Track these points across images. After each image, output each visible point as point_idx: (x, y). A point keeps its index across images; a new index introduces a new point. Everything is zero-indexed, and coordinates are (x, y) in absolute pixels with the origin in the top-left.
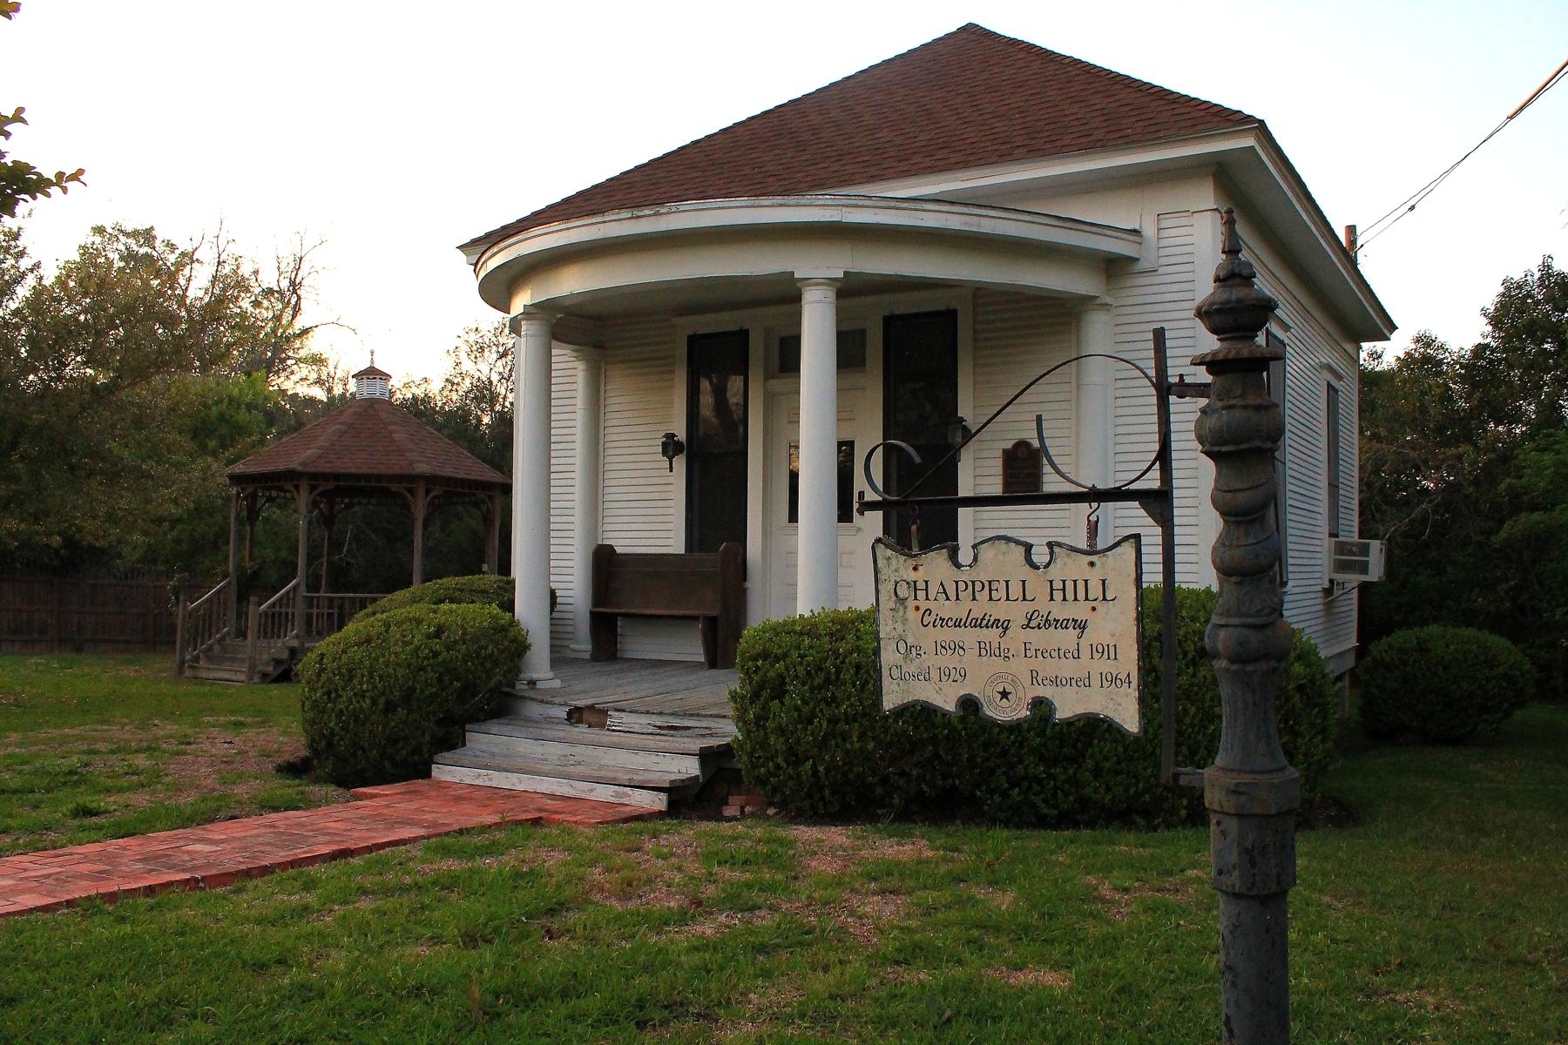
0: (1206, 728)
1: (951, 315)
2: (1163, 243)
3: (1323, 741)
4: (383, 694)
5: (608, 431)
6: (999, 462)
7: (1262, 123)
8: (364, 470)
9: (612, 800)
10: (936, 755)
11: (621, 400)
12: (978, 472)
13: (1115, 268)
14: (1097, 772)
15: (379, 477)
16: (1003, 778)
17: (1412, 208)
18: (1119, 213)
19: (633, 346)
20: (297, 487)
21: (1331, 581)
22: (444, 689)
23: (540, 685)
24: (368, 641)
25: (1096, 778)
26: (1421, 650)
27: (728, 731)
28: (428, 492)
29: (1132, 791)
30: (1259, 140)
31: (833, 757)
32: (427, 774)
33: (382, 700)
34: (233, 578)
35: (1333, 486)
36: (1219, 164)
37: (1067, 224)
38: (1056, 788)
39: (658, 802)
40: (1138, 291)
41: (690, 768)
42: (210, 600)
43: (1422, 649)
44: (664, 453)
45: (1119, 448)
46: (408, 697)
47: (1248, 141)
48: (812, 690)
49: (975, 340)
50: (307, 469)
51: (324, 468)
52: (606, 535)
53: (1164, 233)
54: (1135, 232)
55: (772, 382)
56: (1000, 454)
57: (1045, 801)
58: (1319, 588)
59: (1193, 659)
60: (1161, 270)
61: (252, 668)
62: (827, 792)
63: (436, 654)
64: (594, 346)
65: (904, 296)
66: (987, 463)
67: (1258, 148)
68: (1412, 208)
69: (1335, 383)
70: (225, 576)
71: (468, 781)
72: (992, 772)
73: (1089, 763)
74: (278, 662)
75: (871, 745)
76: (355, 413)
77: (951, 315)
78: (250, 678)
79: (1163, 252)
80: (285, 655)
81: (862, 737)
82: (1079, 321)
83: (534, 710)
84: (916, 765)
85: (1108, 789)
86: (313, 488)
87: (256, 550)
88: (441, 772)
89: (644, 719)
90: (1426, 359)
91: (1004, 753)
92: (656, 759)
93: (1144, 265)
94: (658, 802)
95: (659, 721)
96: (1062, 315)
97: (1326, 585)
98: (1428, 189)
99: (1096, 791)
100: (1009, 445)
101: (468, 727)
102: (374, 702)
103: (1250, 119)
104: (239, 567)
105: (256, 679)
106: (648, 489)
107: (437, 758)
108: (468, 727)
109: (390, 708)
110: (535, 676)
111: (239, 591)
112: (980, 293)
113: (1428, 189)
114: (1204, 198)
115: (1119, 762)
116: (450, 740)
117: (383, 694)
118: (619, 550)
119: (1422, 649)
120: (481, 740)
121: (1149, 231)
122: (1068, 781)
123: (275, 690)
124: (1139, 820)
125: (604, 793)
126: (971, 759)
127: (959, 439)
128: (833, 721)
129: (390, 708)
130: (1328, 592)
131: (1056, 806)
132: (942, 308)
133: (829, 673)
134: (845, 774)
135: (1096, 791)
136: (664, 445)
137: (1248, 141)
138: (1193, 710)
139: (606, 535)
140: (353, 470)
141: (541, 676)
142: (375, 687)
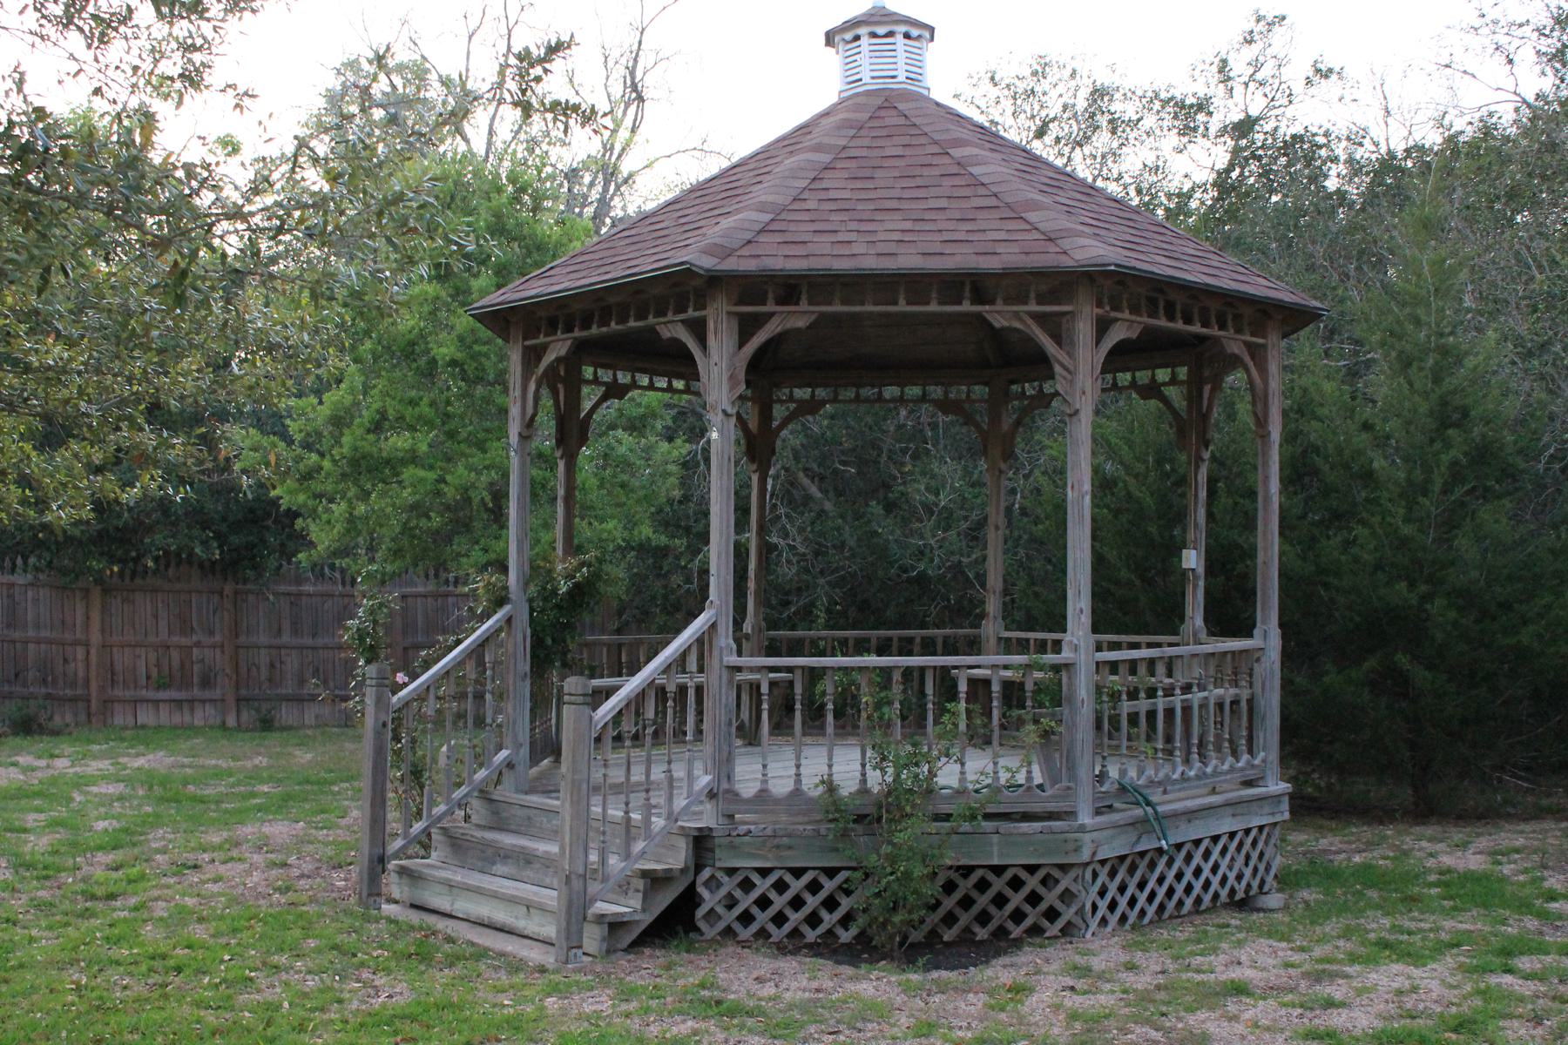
15: (978, 285)
20: (699, 329)
28: (1102, 326)
34: (518, 607)
50: (731, 264)
51: (778, 259)
61: (576, 913)
62: (41, 125)
74: (655, 881)
78: (572, 940)
80: (677, 858)
83: (1099, 759)
86: (747, 326)
87: (584, 529)
104: (537, 571)
105: (592, 939)
111: (537, 643)
123: (647, 970)
124: (1240, 568)
140: (871, 263)
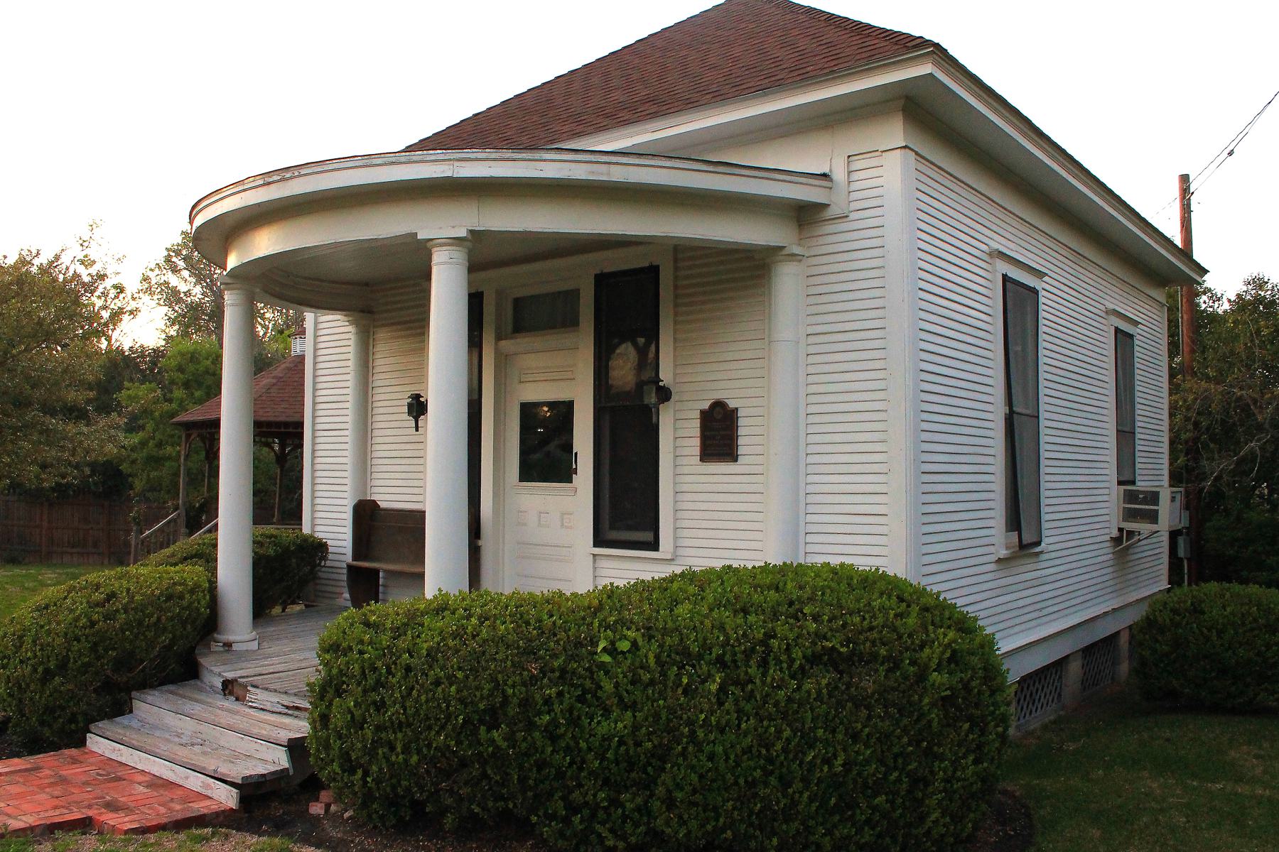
0: (804, 754)
1: (654, 270)
2: (854, 186)
3: (977, 762)
4: (42, 663)
5: (376, 391)
6: (697, 423)
7: (937, 46)
8: (282, 419)
9: (200, 790)
10: (485, 775)
11: (387, 361)
12: (677, 437)
13: (806, 216)
14: (670, 803)
16: (560, 803)
17: (1231, 154)
18: (807, 157)
19: (401, 309)
21: (1121, 530)
22: (98, 658)
23: (235, 647)
24: (47, 607)
25: (669, 809)
26: (1195, 611)
27: (300, 727)
29: (709, 827)
30: (936, 64)
31: (381, 769)
32: (81, 743)
33: (40, 669)
34: (182, 511)
35: (1126, 435)
36: (908, 98)
37: (720, 169)
38: (625, 818)
39: (227, 798)
40: (832, 238)
41: (279, 760)
42: (159, 529)
43: (1197, 610)
44: (410, 413)
45: (812, 409)
46: (63, 666)
47: (925, 69)
48: (365, 691)
49: (676, 297)
52: (375, 490)
53: (855, 176)
54: (825, 175)
55: (503, 343)
56: (697, 415)
57: (611, 831)
58: (1108, 538)
59: (802, 667)
60: (853, 216)
63: (93, 624)
64: (363, 311)
65: (622, 252)
66: (686, 424)
67: (940, 76)
68: (1231, 154)
69: (1124, 326)
70: (176, 509)
71: (108, 754)
72: (550, 795)
73: (660, 791)
75: (415, 759)
76: (289, 369)
77: (654, 270)
79: (854, 196)
81: (406, 750)
82: (769, 270)
84: (466, 784)
85: (683, 822)
88: (97, 744)
89: (275, 698)
90: (1259, 300)
91: (560, 775)
92: (257, 746)
93: (833, 211)
94: (227, 798)
95: (287, 701)
96: (746, 272)
97: (1115, 533)
98: (1243, 134)
99: (667, 824)
100: (706, 405)
101: (134, 694)
102: (35, 670)
103: (922, 43)
106: (403, 447)
107: (92, 727)
108: (134, 694)
109: (48, 675)
110: (231, 638)
112: (682, 251)
113: (1243, 134)
114: (893, 133)
115: (695, 791)
116: (115, 704)
117: (42, 663)
118: (383, 505)
119: (1197, 610)
120: (153, 709)
121: (839, 175)
122: (638, 809)
125: (195, 782)
126: (523, 780)
127: (653, 400)
128: (379, 728)
129: (48, 675)
130: (1117, 541)
131: (624, 838)
132: (647, 264)
133: (380, 674)
134: (394, 788)
135: (667, 824)
136: (410, 405)
137: (925, 69)
138: (787, 733)
139: (375, 490)
141: (237, 638)
142: (36, 656)
